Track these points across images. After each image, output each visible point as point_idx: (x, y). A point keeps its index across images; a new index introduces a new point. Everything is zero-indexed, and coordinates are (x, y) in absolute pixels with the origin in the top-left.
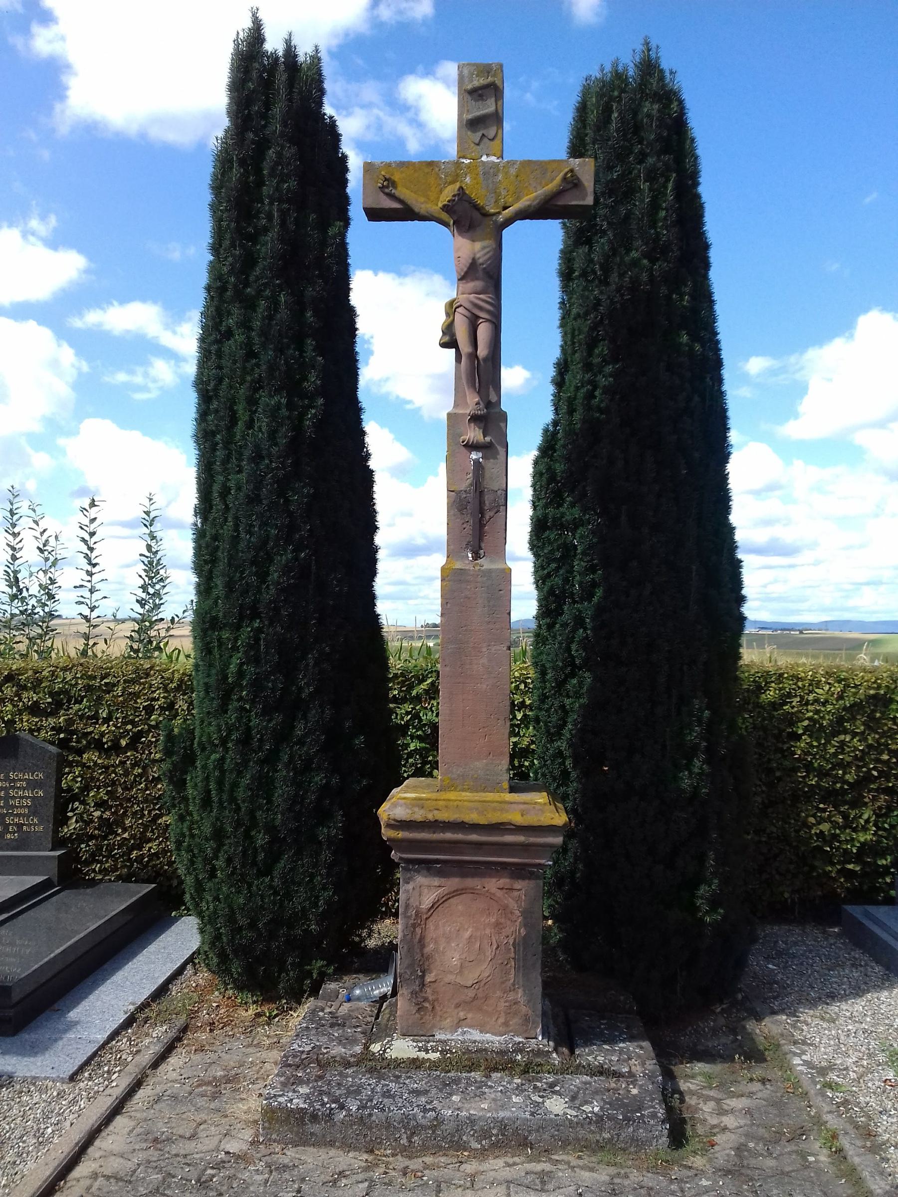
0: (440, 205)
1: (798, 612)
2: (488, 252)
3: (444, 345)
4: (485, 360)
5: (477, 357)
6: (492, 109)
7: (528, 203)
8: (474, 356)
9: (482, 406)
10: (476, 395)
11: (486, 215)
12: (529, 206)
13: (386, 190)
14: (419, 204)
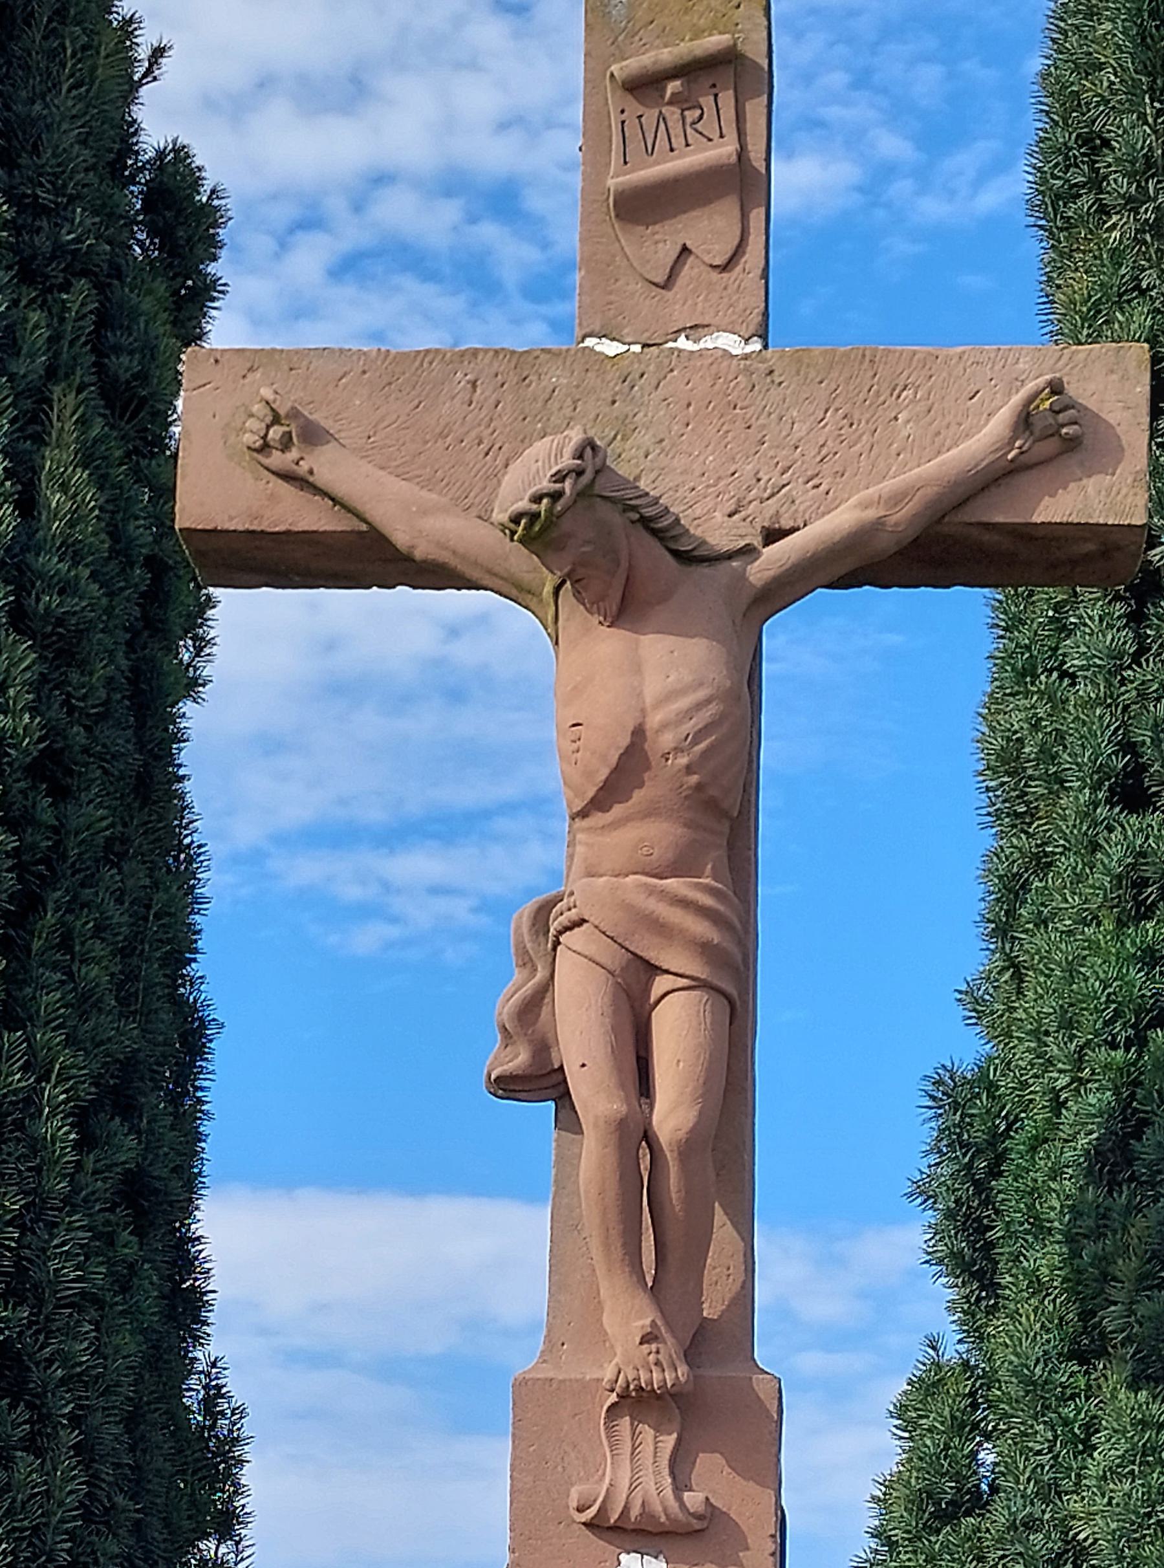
0: (501, 516)
1: (183, 479)
2: (708, 701)
3: (508, 1086)
4: (688, 1148)
5: (648, 1136)
6: (725, 150)
7: (871, 514)
8: (635, 1135)
9: (669, 1347)
10: (643, 1300)
11: (693, 557)
12: (876, 526)
13: (277, 459)
14: (410, 514)
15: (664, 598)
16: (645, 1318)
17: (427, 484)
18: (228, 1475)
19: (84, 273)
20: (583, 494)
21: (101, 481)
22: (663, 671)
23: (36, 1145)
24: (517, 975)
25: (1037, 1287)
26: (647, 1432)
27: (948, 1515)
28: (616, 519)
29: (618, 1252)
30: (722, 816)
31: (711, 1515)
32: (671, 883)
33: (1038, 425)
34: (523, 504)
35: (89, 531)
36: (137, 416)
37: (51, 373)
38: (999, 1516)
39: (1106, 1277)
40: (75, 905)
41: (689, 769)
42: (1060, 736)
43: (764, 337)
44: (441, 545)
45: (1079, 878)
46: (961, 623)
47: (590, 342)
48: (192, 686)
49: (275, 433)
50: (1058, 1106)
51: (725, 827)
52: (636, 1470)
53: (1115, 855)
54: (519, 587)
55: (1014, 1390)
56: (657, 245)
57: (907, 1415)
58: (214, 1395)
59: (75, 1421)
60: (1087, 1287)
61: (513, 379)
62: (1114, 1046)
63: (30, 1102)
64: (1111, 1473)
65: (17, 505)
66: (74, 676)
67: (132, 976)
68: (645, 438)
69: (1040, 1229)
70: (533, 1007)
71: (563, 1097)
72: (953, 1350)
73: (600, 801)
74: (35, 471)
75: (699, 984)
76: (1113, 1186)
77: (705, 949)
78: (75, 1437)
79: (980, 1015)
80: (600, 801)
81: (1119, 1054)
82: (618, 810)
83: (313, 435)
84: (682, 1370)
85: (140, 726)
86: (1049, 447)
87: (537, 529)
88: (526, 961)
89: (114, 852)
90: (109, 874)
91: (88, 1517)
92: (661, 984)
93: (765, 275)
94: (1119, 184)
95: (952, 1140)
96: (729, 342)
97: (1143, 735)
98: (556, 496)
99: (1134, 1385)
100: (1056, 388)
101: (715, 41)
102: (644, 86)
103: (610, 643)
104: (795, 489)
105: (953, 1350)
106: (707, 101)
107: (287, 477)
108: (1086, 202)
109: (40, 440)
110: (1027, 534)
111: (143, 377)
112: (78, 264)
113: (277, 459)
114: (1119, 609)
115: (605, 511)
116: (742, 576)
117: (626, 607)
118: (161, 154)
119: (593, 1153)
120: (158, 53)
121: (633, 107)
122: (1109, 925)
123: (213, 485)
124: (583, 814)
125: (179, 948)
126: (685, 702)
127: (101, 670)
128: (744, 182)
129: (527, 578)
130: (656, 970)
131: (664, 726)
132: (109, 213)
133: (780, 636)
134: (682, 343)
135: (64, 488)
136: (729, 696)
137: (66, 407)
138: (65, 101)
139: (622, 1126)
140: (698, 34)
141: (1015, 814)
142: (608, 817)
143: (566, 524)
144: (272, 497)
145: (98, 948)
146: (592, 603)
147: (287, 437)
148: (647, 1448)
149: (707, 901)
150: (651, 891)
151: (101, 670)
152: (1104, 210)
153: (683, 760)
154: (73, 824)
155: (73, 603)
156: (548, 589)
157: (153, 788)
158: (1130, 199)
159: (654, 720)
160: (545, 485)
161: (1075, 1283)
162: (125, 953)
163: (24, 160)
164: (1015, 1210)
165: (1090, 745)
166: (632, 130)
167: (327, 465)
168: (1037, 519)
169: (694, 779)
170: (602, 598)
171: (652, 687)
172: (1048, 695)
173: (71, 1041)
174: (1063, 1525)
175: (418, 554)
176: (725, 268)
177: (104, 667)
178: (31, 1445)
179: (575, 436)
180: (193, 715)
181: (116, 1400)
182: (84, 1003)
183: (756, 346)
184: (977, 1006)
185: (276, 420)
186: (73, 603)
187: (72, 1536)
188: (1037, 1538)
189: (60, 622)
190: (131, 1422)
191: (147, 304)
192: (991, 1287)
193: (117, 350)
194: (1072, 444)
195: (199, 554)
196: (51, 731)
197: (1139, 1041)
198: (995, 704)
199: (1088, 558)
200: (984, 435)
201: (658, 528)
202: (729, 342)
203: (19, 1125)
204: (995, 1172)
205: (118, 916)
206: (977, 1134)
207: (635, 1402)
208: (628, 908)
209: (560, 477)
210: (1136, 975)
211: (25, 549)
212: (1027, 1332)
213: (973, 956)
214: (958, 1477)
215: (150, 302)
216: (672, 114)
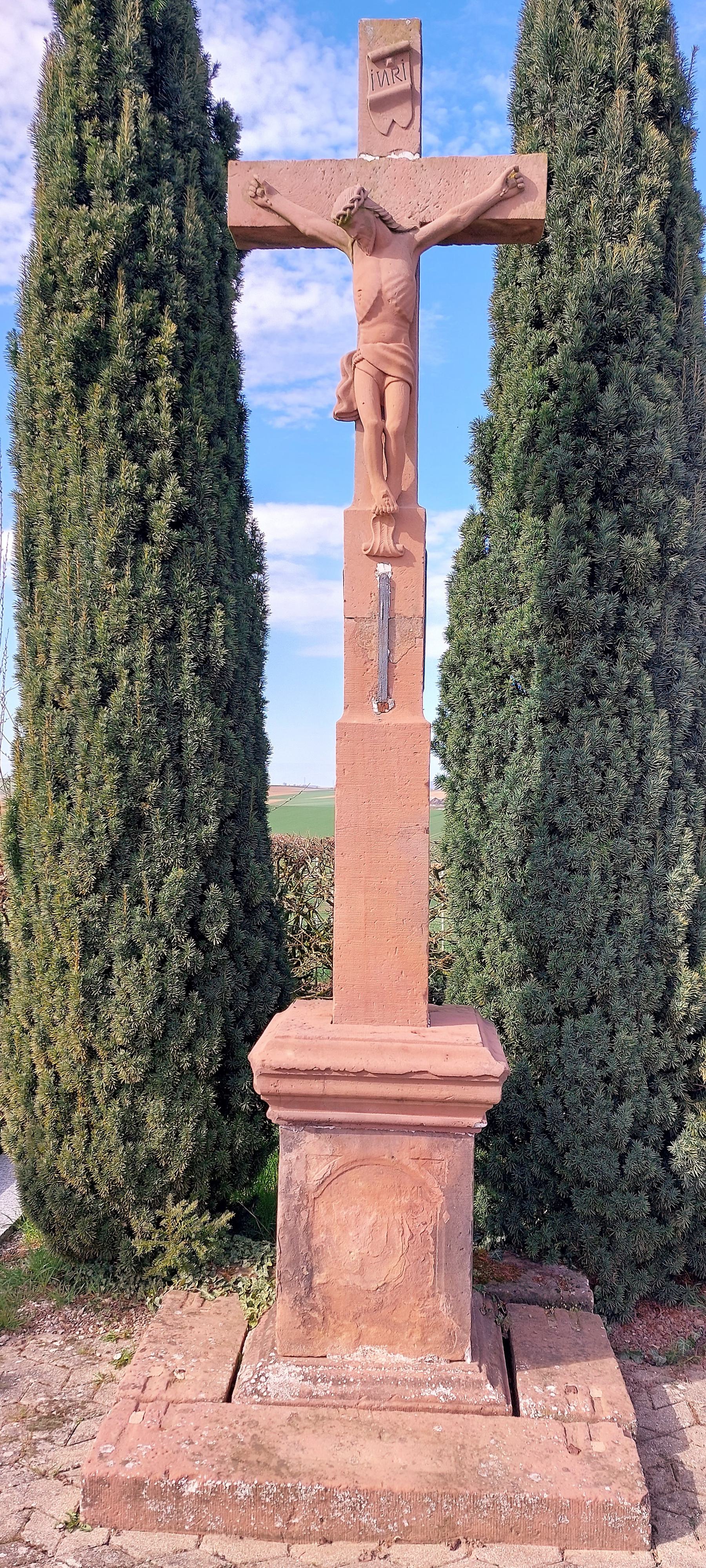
4: (397, 434)
5: (384, 431)
6: (406, 84)
7: (455, 216)
9: (392, 499)
10: (384, 484)
12: (458, 219)
13: (260, 200)
15: (387, 245)
16: (384, 489)
17: (310, 208)
18: (260, 554)
19: (195, 146)
20: (361, 207)
21: (204, 220)
22: (387, 271)
23: (195, 445)
24: (342, 378)
25: (504, 486)
26: (385, 526)
27: (475, 560)
28: (371, 216)
29: (375, 469)
30: (408, 322)
31: (404, 551)
32: (391, 345)
33: (510, 183)
34: (341, 211)
35: (201, 237)
36: (214, 194)
37: (186, 181)
38: (491, 558)
39: (526, 482)
40: (203, 367)
41: (396, 305)
42: (516, 305)
43: (420, 153)
44: (314, 229)
45: (521, 352)
46: (484, 256)
47: (362, 156)
48: (237, 296)
49: (259, 191)
50: (512, 429)
51: (408, 326)
52: (382, 538)
53: (532, 344)
54: (340, 243)
55: (497, 520)
56: (384, 120)
57: (464, 531)
58: (254, 530)
59: (213, 533)
60: (519, 486)
61: (337, 170)
62: (530, 408)
63: (192, 431)
64: (526, 543)
65: (177, 228)
66: (199, 289)
67: (222, 392)
68: (381, 190)
69: (505, 468)
70: (347, 389)
71: (358, 419)
72: (478, 509)
73: (367, 318)
74: (182, 216)
75: (400, 379)
76: (529, 452)
77: (403, 368)
78: (213, 538)
79: (489, 402)
80: (367, 318)
81: (532, 411)
82: (374, 320)
83: (271, 191)
84: (396, 505)
85: (221, 308)
86: (514, 191)
87: (345, 221)
88: (345, 374)
89: (214, 349)
90: (213, 357)
91: (218, 561)
92: (388, 380)
93: (420, 131)
94: (539, 106)
95: (479, 442)
96: (408, 155)
97: (542, 302)
98: (351, 208)
99: (533, 516)
100: (516, 170)
101: (403, 43)
102: (378, 61)
103: (370, 261)
104: (430, 208)
105: (478, 509)
106: (400, 66)
107: (263, 207)
108: (527, 114)
109: (183, 205)
110: (506, 223)
111: (216, 183)
112: (193, 142)
113: (260, 200)
114: (535, 259)
115: (367, 213)
116: (413, 238)
117: (375, 249)
118: (219, 105)
119: (367, 436)
120: (216, 66)
121: (375, 69)
122: (530, 367)
123: (239, 211)
124: (362, 322)
125: (237, 385)
126: (395, 281)
127: (207, 286)
128: (412, 96)
129: (343, 240)
130: (386, 375)
131: (388, 290)
132: (202, 124)
133: (426, 257)
134: (393, 156)
135: (192, 222)
136: (409, 279)
137: (192, 193)
138: (185, 82)
139: (376, 426)
140: (397, 40)
141: (501, 332)
142: (370, 323)
143: (355, 218)
144: (259, 214)
145: (211, 381)
146: (364, 247)
147: (262, 192)
148: (385, 531)
149: (403, 351)
150: (385, 348)
151: (207, 286)
152: (533, 116)
153: (394, 302)
154: (201, 339)
155: (197, 263)
156: (350, 244)
157: (224, 328)
158: (542, 111)
159: (385, 288)
160: (348, 204)
161: (515, 486)
162: (220, 384)
163: (174, 104)
164: (498, 462)
165: (525, 308)
166: (375, 76)
167: (276, 202)
168: (510, 217)
169: (398, 308)
170: (367, 245)
171: (384, 276)
172: (512, 290)
173: (204, 412)
174: (510, 560)
175: (307, 233)
176: (407, 128)
177: (208, 286)
178: (200, 539)
179: (358, 187)
180: (238, 306)
181: (224, 527)
182: (207, 399)
183: (417, 156)
184: (488, 401)
185: (259, 186)
186: (197, 263)
187: (214, 567)
188: (502, 564)
189: (193, 269)
190: (230, 534)
191: (216, 157)
192: (490, 489)
193: (207, 174)
194: (521, 190)
195: (236, 236)
196: (192, 307)
197: (539, 405)
198: (496, 295)
199: (526, 232)
200: (492, 188)
201: (384, 220)
202: (408, 155)
203: (190, 439)
204: (492, 452)
205: (216, 370)
206: (487, 441)
207: (382, 516)
208: (377, 354)
209: (353, 201)
210: (538, 384)
211: (180, 243)
212: (501, 501)
213: (487, 382)
214: (479, 548)
215: (217, 155)
216: (388, 71)
